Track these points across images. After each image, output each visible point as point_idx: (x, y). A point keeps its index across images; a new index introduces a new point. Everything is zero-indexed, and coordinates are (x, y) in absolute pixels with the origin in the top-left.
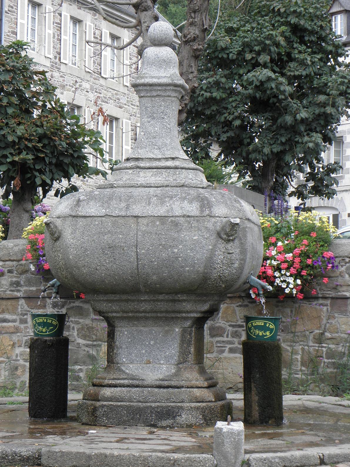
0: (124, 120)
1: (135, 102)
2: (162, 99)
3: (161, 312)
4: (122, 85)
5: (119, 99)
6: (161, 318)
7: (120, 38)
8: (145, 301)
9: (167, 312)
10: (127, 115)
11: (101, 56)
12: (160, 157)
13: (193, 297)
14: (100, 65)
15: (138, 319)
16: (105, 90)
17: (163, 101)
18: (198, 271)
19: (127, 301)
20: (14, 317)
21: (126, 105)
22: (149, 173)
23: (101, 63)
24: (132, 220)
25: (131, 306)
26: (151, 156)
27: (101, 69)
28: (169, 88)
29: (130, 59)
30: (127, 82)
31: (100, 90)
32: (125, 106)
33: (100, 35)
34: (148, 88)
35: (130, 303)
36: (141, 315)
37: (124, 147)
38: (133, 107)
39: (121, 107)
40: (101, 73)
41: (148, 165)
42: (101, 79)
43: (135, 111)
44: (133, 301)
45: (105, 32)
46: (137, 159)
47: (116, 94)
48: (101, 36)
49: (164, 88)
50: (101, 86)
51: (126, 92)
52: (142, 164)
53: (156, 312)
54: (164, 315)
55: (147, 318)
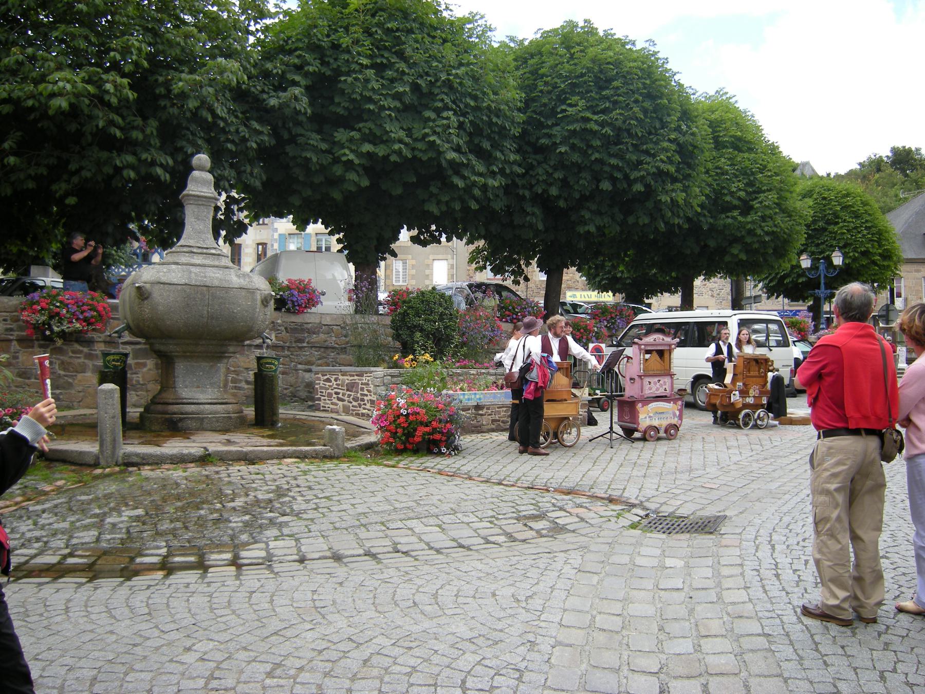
13: (235, 343)
22: (200, 257)
24: (205, 288)
41: (200, 251)
52: (195, 250)
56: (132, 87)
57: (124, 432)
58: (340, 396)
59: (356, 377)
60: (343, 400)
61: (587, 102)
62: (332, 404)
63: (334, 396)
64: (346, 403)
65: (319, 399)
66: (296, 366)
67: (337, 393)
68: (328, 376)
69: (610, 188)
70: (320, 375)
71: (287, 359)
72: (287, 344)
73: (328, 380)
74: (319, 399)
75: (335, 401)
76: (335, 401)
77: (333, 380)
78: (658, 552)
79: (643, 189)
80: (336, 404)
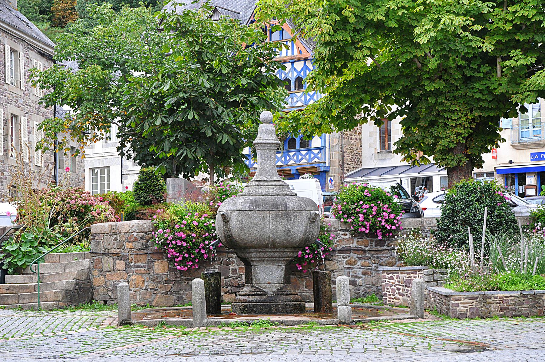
0: (22, 117)
1: (28, 103)
2: (270, 150)
3: (276, 257)
4: (19, 89)
5: (17, 101)
6: (276, 260)
7: (17, 51)
8: (269, 252)
9: (279, 257)
10: (23, 113)
11: (5, 66)
12: (271, 180)
14: (5, 74)
15: (263, 261)
16: (8, 93)
17: (270, 151)
18: (300, 237)
19: (259, 252)
20: (144, 265)
21: (22, 105)
23: (5, 71)
25: (261, 255)
26: (266, 179)
27: (5, 76)
28: (274, 145)
29: (25, 68)
30: (23, 87)
31: (5, 93)
32: (22, 106)
33: (3, 49)
34: (263, 145)
35: (261, 253)
36: (265, 259)
37: (23, 138)
38: (27, 106)
39: (19, 107)
40: (5, 80)
41: (266, 184)
42: (5, 85)
43: (28, 109)
44: (263, 252)
45: (7, 47)
46: (260, 181)
47: (16, 97)
48: (4, 50)
49: (271, 145)
50: (6, 90)
51: (22, 95)
52: (262, 184)
53: (274, 258)
54: (277, 259)
55: (268, 261)
56: (468, 57)
57: (4, 283)
58: (401, 291)
59: (412, 275)
60: (403, 295)
61: (380, 110)
62: (395, 298)
63: (397, 291)
64: (405, 297)
65: (385, 295)
66: (376, 267)
67: (398, 289)
68: (391, 275)
69: (284, 158)
70: (385, 274)
71: (369, 261)
72: (368, 248)
73: (391, 278)
74: (385, 295)
75: (397, 296)
76: (397, 296)
77: (395, 277)
78: (36, 300)
79: (284, 158)
80: (398, 299)
